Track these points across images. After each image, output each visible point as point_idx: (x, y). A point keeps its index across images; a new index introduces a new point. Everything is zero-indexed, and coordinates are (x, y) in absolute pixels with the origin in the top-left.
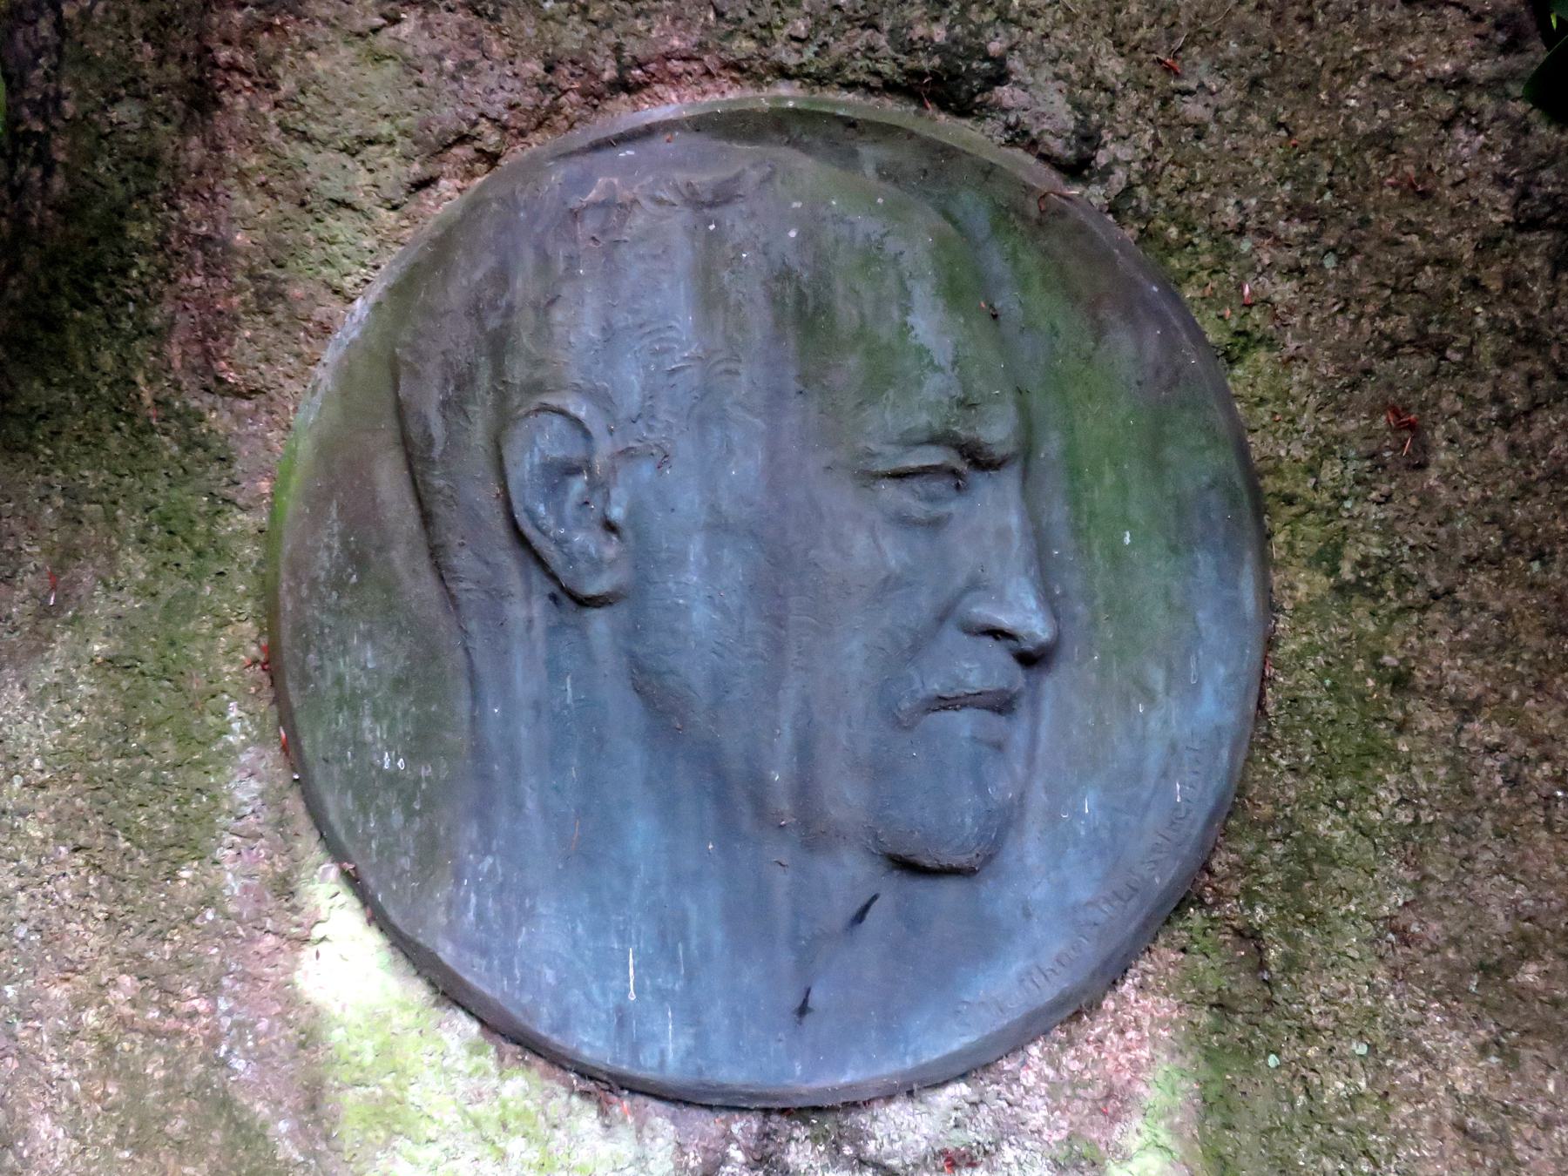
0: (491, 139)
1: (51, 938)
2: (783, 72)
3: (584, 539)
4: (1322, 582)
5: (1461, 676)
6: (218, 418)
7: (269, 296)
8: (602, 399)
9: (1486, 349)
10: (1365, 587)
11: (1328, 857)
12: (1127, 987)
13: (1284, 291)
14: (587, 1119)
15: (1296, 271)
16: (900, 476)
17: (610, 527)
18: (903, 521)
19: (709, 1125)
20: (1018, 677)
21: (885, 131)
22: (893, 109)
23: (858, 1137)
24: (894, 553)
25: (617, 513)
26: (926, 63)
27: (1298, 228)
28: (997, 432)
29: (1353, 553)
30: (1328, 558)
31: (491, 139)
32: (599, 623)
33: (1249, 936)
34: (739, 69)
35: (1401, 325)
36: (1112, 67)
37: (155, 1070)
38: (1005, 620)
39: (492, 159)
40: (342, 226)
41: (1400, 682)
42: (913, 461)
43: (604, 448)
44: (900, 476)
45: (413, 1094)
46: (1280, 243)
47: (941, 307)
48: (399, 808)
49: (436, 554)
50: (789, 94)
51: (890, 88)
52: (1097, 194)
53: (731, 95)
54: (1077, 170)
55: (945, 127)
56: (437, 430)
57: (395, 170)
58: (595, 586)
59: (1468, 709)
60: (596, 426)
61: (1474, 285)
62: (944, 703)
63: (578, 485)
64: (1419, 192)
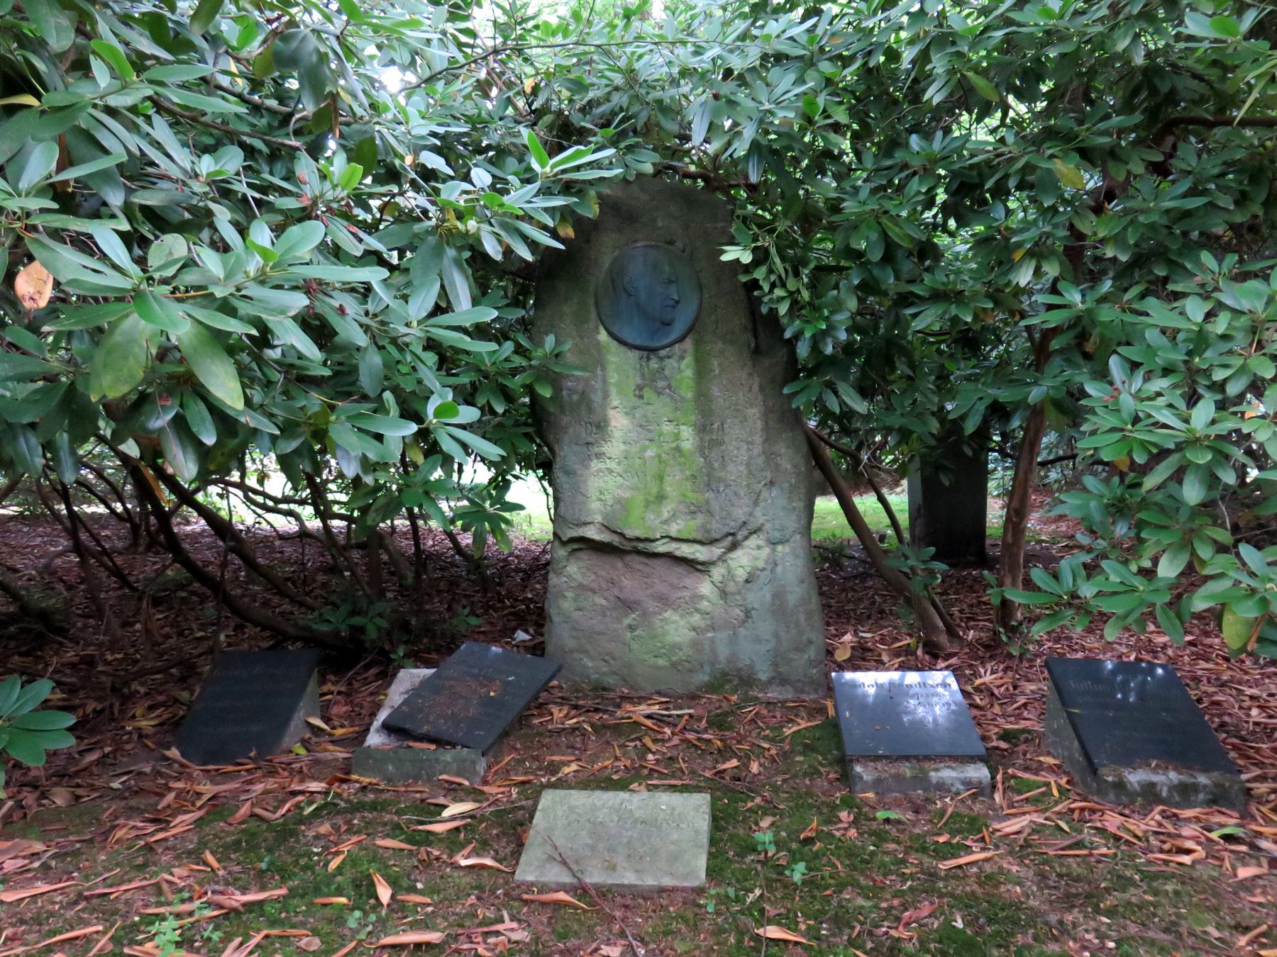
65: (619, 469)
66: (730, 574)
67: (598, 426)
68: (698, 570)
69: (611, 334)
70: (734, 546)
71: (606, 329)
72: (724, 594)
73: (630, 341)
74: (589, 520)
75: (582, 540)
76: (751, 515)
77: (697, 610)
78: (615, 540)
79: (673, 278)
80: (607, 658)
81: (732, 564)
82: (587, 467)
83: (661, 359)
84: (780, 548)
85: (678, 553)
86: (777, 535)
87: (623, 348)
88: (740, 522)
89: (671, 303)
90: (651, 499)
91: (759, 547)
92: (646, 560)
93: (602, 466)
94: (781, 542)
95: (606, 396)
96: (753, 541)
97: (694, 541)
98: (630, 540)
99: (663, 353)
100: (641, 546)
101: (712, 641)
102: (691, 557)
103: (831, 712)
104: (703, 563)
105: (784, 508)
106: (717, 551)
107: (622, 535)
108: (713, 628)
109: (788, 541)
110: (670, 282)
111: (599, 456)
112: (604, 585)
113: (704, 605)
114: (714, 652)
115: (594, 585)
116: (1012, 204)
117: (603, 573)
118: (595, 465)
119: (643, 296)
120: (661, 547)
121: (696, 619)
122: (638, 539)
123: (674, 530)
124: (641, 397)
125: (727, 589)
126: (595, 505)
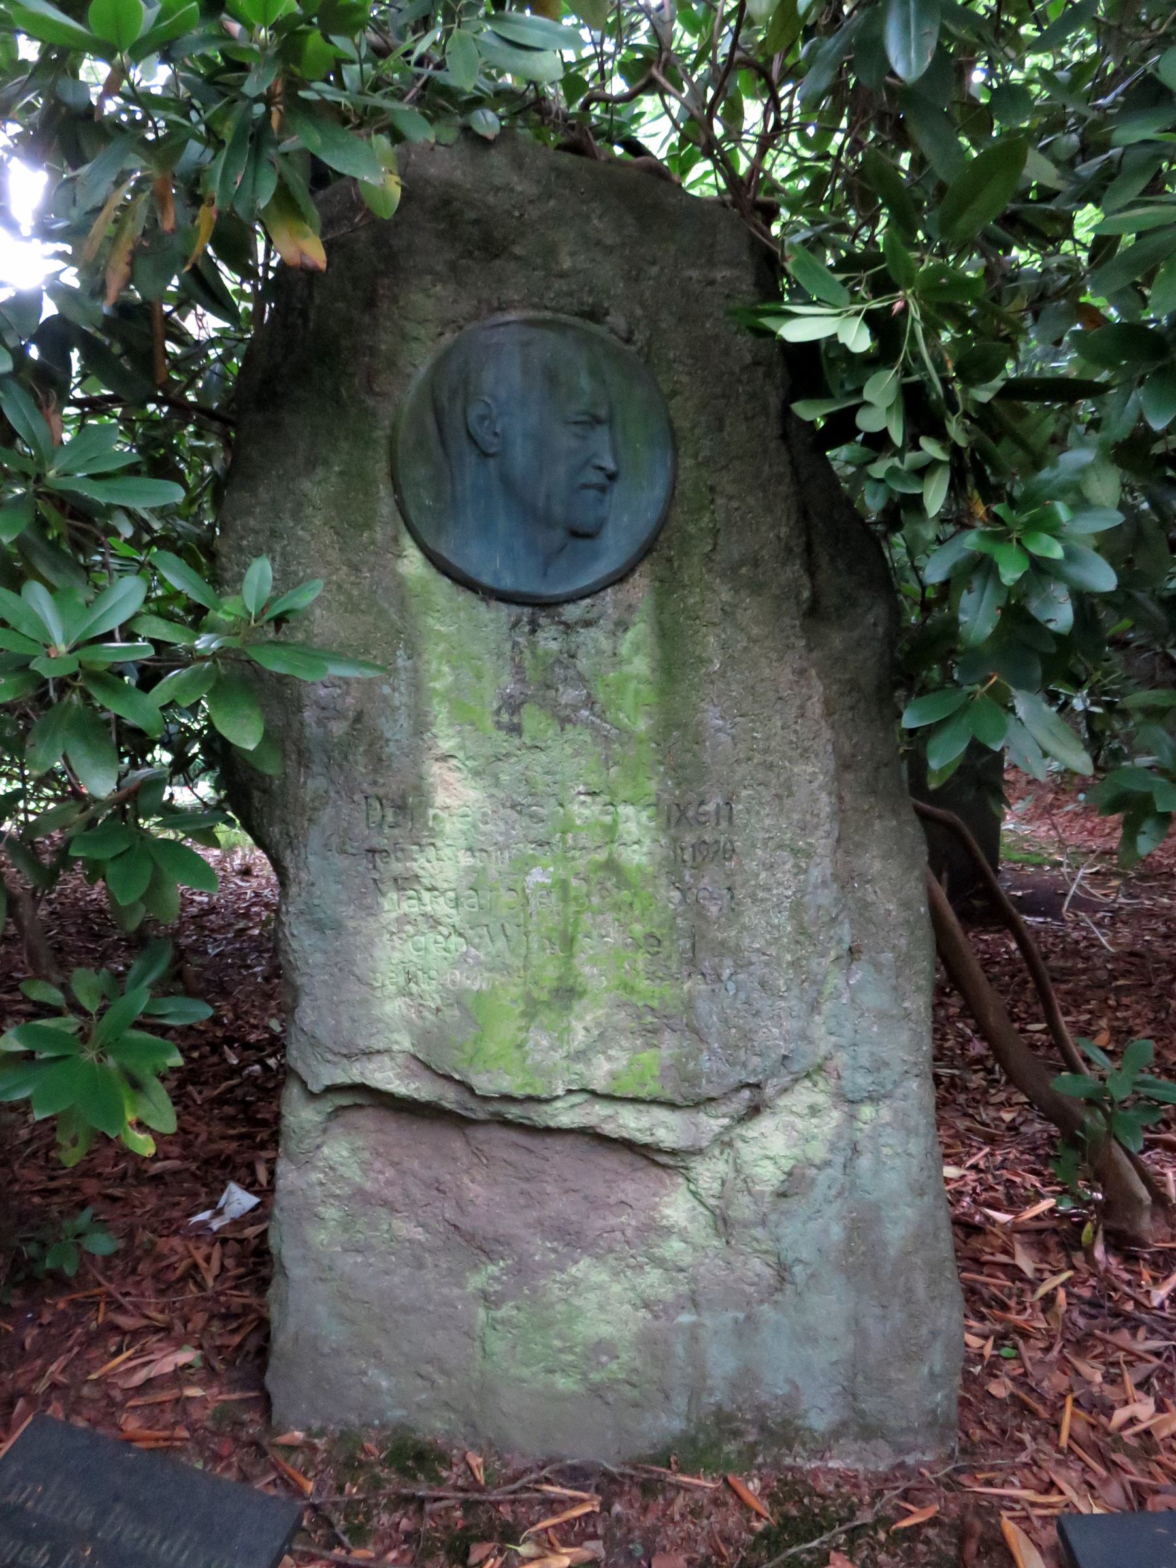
0: (462, 322)
1: (322, 555)
2: (546, 308)
3: (490, 438)
4: (693, 462)
5: (730, 489)
6: (370, 402)
7: (391, 364)
8: (494, 398)
9: (742, 398)
10: (706, 463)
11: (692, 537)
12: (637, 575)
13: (685, 379)
14: (482, 607)
15: (689, 374)
16: (576, 423)
17: (496, 434)
18: (576, 436)
19: (516, 610)
20: (607, 482)
21: (573, 327)
22: (576, 321)
23: (560, 615)
24: (574, 443)
25: (498, 430)
26: (586, 308)
27: (690, 361)
28: (602, 412)
29: (702, 454)
30: (695, 456)
31: (462, 322)
32: (492, 463)
33: (669, 560)
34: (535, 307)
35: (718, 390)
36: (639, 312)
37: (355, 592)
38: (603, 465)
39: (461, 328)
40: (414, 345)
41: (712, 489)
42: (579, 418)
43: (495, 411)
44: (576, 423)
45: (433, 598)
46: (685, 365)
47: (816, 708)
48: (746, 126)
49: (443, 443)
50: (548, 315)
51: (576, 314)
52: (633, 348)
53: (531, 314)
54: (628, 341)
55: (592, 327)
56: (446, 404)
57: (434, 329)
58: (492, 450)
59: (731, 498)
60: (493, 405)
61: (740, 381)
62: (586, 486)
63: (487, 423)
64: (726, 353)
68: (665, 1167)
70: (754, 1111)
72: (723, 1223)
73: (486, 580)
74: (377, 1044)
78: (450, 1098)
81: (748, 1152)
83: (568, 627)
84: (867, 1112)
85: (609, 1129)
87: (464, 598)
89: (597, 478)
91: (814, 1110)
93: (410, 907)
98: (486, 1099)
100: (513, 1112)
101: (693, 1334)
104: (673, 1153)
106: (712, 1123)
108: (694, 1302)
110: (596, 421)
113: (674, 1247)
114: (697, 1361)
118: (393, 905)
119: (520, 456)
120: (565, 1115)
121: (652, 1280)
122: (507, 1098)
123: (599, 1073)
126: (394, 1008)
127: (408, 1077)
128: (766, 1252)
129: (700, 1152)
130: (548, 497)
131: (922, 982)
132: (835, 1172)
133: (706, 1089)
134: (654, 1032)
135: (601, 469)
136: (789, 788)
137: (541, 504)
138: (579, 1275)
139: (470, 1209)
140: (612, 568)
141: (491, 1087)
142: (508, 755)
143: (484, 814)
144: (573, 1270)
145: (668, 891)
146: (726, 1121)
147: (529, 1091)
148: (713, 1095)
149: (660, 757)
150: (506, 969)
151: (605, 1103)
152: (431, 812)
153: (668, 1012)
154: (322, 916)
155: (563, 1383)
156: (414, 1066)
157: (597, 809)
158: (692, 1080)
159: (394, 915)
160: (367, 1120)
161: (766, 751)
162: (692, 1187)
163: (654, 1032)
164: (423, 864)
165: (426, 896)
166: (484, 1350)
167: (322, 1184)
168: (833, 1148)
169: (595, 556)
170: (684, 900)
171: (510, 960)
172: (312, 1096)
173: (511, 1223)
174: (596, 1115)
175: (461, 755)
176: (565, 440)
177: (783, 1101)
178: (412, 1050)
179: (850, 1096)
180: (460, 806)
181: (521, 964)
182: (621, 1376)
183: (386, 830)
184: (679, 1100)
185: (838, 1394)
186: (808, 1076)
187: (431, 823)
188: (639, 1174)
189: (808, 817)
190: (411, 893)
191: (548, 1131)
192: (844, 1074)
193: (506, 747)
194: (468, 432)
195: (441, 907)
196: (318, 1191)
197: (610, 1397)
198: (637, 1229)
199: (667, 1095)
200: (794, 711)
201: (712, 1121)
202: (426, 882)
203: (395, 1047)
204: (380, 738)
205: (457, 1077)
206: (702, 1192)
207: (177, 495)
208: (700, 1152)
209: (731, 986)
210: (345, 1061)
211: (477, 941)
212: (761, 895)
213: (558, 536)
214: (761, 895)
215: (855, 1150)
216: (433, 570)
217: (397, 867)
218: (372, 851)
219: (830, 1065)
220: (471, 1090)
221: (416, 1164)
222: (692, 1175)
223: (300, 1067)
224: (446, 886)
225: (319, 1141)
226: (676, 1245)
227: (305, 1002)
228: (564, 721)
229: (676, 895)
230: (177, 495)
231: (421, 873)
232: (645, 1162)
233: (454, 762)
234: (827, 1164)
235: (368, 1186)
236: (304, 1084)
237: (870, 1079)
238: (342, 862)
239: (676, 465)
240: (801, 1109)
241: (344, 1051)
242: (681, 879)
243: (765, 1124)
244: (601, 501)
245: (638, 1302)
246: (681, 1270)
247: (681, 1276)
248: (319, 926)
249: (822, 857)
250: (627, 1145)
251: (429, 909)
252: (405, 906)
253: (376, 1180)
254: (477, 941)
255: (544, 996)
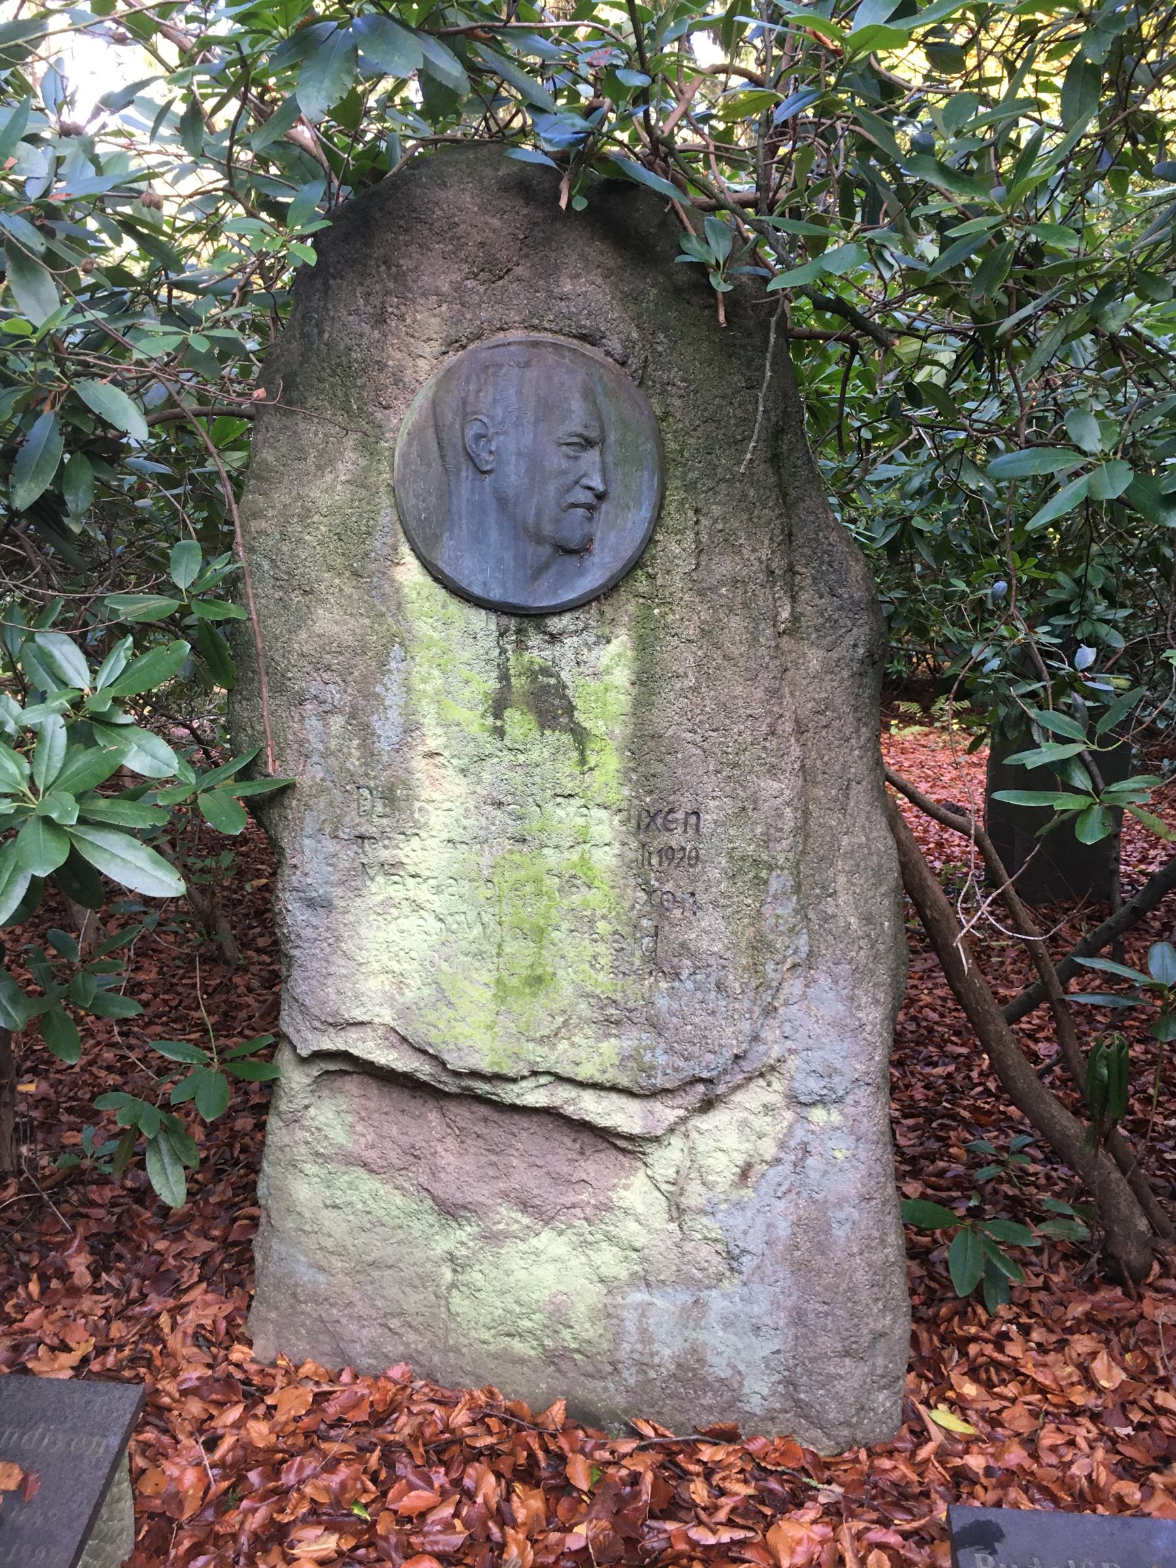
3: (485, 455)
16: (567, 444)
17: (491, 452)
19: (505, 620)
20: (595, 502)
24: (565, 464)
32: (488, 479)
38: (592, 484)
43: (491, 431)
44: (567, 444)
51: (575, 337)
55: (587, 348)
65: (438, 903)
66: (694, 1167)
67: (389, 797)
68: (623, 1151)
69: (429, 567)
70: (707, 1105)
71: (419, 556)
72: (677, 1211)
73: (477, 590)
74: (358, 1014)
75: (345, 1056)
76: (756, 1038)
77: (610, 1238)
78: (423, 1069)
79: (593, 434)
80: (394, 1323)
81: (703, 1144)
82: (358, 892)
83: (554, 638)
84: (818, 1115)
85: (569, 1110)
86: (814, 1085)
87: (456, 608)
88: (728, 1054)
89: (586, 497)
90: (514, 982)
91: (768, 1109)
92: (496, 1116)
93: (396, 892)
94: (821, 1102)
95: (411, 728)
96: (755, 1096)
97: (615, 1089)
98: (457, 1074)
99: (555, 624)
100: (482, 1087)
101: (644, 1310)
102: (603, 1122)
103: (935, 1339)
104: (630, 1138)
105: (839, 1026)
106: (666, 1113)
107: (437, 1060)
108: (645, 1281)
109: (839, 1100)
110: (588, 443)
111: (391, 868)
112: (393, 1156)
113: (630, 1230)
114: (646, 1336)
115: (371, 1155)
116: (719, 250)
117: (394, 1131)
118: (379, 888)
119: (513, 474)
120: (535, 1096)
121: (608, 1260)
122: (475, 1074)
123: (560, 1057)
124: (500, 732)
125: (685, 1202)
126: (374, 985)
127: (387, 1047)
128: (716, 1240)
129: (657, 1139)
130: (539, 514)
131: (881, 996)
132: (786, 1168)
133: (659, 1081)
134: (617, 1023)
135: (590, 488)
136: (755, 802)
137: (531, 519)
138: (541, 1248)
139: (442, 1175)
140: (597, 584)
141: (461, 1064)
142: (490, 755)
143: (467, 810)
144: (534, 1242)
145: (634, 891)
146: (681, 1112)
147: (496, 1069)
148: (668, 1086)
149: (632, 765)
150: (479, 955)
151: (568, 1087)
152: (417, 805)
153: (630, 1005)
154: (314, 894)
155: (518, 1346)
156: (394, 1038)
157: (572, 810)
158: (648, 1070)
159: (379, 898)
160: (351, 1085)
161: (735, 765)
162: (649, 1172)
163: (617, 1023)
164: (409, 852)
165: (411, 882)
166: (449, 1310)
167: (307, 1143)
168: (782, 1146)
169: (581, 572)
170: (649, 900)
171: (486, 947)
172: (303, 1061)
173: (479, 1193)
174: (560, 1097)
175: (446, 753)
176: (556, 460)
177: (738, 1097)
178: (393, 1024)
179: (803, 1099)
180: (444, 801)
181: (494, 952)
182: (574, 1346)
183: (375, 819)
184: (636, 1090)
185: (779, 1383)
186: (762, 1075)
187: (416, 815)
188: (602, 1155)
189: (772, 831)
190: (396, 878)
191: (514, 1109)
192: (798, 1076)
193: (489, 749)
194: (465, 449)
195: (422, 893)
196: (303, 1149)
197: (564, 1366)
198: (596, 1207)
199: (625, 1082)
200: (764, 728)
201: (668, 1111)
202: (411, 869)
203: (377, 1020)
204: (373, 734)
205: (431, 1051)
206: (657, 1177)
207: (212, 1200)
208: (657, 1139)
209: (689, 985)
210: (331, 1029)
211: (455, 926)
212: (722, 901)
213: (546, 550)
214: (722, 901)
215: (807, 1152)
216: (429, 579)
217: (385, 854)
218: (362, 837)
219: (784, 1068)
220: (443, 1064)
221: (394, 1131)
222: (649, 1160)
223: (290, 1031)
224: (428, 873)
225: (307, 1102)
226: (633, 1226)
227: (296, 973)
228: (1054, 445)
229: (642, 896)
230: (212, 1200)
231: (405, 860)
232: (605, 1145)
233: (441, 759)
234: (778, 1161)
235: (350, 1146)
236: (294, 1048)
237: (822, 1084)
238: (331, 846)
239: (663, 488)
240: (755, 1105)
241: (330, 1020)
242: (647, 883)
243: (718, 1118)
244: (590, 519)
245: (596, 1278)
246: (636, 1250)
247: (634, 1255)
248: (311, 904)
249: (782, 869)
250: (584, 1127)
251: (411, 894)
252: (391, 890)
253: (356, 1142)
254: (455, 926)
255: (514, 982)
